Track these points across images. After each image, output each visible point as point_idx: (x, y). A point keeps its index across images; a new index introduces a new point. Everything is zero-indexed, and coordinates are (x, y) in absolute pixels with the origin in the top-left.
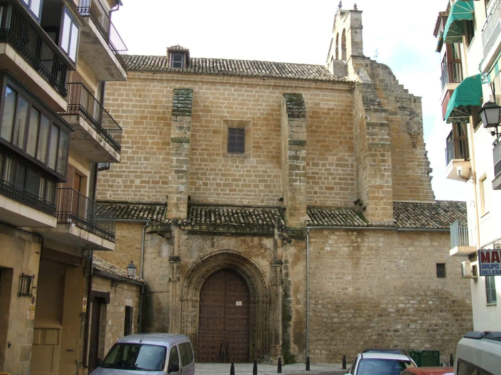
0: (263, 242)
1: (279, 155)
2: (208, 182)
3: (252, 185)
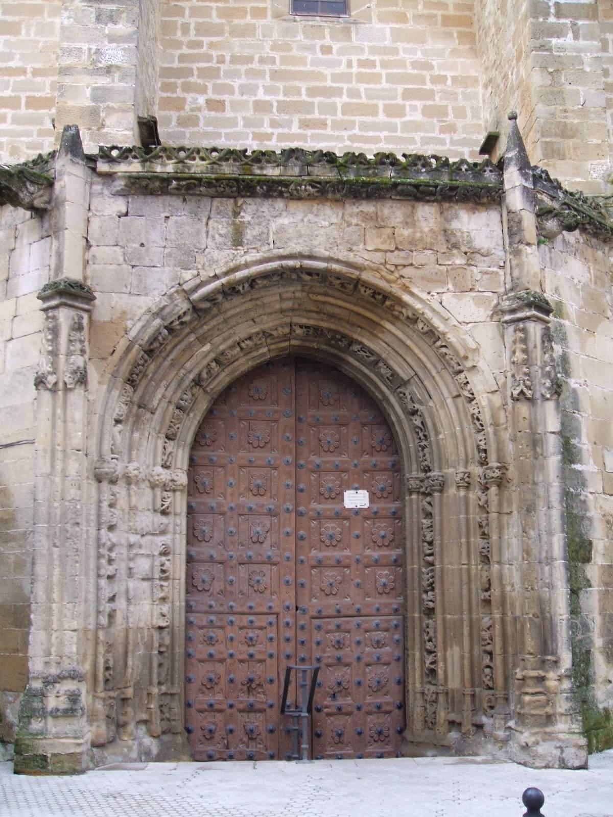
0: (455, 225)
1: (467, 13)
2: (226, 97)
3: (381, 107)
